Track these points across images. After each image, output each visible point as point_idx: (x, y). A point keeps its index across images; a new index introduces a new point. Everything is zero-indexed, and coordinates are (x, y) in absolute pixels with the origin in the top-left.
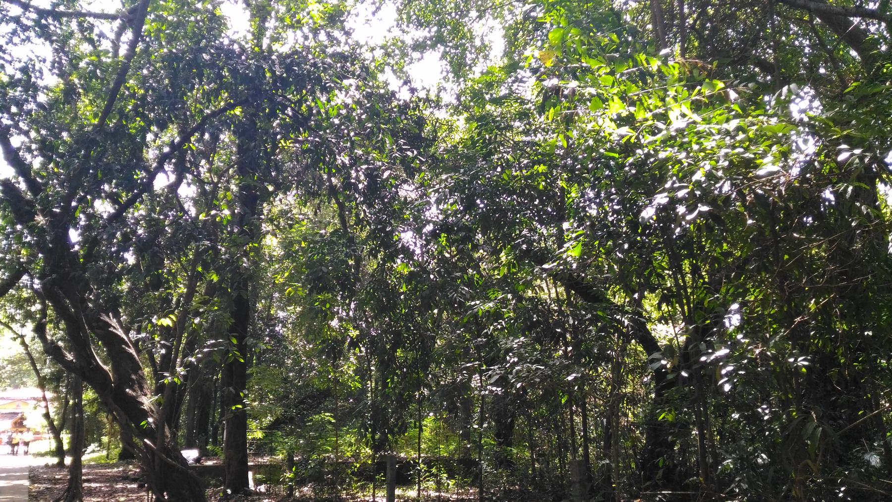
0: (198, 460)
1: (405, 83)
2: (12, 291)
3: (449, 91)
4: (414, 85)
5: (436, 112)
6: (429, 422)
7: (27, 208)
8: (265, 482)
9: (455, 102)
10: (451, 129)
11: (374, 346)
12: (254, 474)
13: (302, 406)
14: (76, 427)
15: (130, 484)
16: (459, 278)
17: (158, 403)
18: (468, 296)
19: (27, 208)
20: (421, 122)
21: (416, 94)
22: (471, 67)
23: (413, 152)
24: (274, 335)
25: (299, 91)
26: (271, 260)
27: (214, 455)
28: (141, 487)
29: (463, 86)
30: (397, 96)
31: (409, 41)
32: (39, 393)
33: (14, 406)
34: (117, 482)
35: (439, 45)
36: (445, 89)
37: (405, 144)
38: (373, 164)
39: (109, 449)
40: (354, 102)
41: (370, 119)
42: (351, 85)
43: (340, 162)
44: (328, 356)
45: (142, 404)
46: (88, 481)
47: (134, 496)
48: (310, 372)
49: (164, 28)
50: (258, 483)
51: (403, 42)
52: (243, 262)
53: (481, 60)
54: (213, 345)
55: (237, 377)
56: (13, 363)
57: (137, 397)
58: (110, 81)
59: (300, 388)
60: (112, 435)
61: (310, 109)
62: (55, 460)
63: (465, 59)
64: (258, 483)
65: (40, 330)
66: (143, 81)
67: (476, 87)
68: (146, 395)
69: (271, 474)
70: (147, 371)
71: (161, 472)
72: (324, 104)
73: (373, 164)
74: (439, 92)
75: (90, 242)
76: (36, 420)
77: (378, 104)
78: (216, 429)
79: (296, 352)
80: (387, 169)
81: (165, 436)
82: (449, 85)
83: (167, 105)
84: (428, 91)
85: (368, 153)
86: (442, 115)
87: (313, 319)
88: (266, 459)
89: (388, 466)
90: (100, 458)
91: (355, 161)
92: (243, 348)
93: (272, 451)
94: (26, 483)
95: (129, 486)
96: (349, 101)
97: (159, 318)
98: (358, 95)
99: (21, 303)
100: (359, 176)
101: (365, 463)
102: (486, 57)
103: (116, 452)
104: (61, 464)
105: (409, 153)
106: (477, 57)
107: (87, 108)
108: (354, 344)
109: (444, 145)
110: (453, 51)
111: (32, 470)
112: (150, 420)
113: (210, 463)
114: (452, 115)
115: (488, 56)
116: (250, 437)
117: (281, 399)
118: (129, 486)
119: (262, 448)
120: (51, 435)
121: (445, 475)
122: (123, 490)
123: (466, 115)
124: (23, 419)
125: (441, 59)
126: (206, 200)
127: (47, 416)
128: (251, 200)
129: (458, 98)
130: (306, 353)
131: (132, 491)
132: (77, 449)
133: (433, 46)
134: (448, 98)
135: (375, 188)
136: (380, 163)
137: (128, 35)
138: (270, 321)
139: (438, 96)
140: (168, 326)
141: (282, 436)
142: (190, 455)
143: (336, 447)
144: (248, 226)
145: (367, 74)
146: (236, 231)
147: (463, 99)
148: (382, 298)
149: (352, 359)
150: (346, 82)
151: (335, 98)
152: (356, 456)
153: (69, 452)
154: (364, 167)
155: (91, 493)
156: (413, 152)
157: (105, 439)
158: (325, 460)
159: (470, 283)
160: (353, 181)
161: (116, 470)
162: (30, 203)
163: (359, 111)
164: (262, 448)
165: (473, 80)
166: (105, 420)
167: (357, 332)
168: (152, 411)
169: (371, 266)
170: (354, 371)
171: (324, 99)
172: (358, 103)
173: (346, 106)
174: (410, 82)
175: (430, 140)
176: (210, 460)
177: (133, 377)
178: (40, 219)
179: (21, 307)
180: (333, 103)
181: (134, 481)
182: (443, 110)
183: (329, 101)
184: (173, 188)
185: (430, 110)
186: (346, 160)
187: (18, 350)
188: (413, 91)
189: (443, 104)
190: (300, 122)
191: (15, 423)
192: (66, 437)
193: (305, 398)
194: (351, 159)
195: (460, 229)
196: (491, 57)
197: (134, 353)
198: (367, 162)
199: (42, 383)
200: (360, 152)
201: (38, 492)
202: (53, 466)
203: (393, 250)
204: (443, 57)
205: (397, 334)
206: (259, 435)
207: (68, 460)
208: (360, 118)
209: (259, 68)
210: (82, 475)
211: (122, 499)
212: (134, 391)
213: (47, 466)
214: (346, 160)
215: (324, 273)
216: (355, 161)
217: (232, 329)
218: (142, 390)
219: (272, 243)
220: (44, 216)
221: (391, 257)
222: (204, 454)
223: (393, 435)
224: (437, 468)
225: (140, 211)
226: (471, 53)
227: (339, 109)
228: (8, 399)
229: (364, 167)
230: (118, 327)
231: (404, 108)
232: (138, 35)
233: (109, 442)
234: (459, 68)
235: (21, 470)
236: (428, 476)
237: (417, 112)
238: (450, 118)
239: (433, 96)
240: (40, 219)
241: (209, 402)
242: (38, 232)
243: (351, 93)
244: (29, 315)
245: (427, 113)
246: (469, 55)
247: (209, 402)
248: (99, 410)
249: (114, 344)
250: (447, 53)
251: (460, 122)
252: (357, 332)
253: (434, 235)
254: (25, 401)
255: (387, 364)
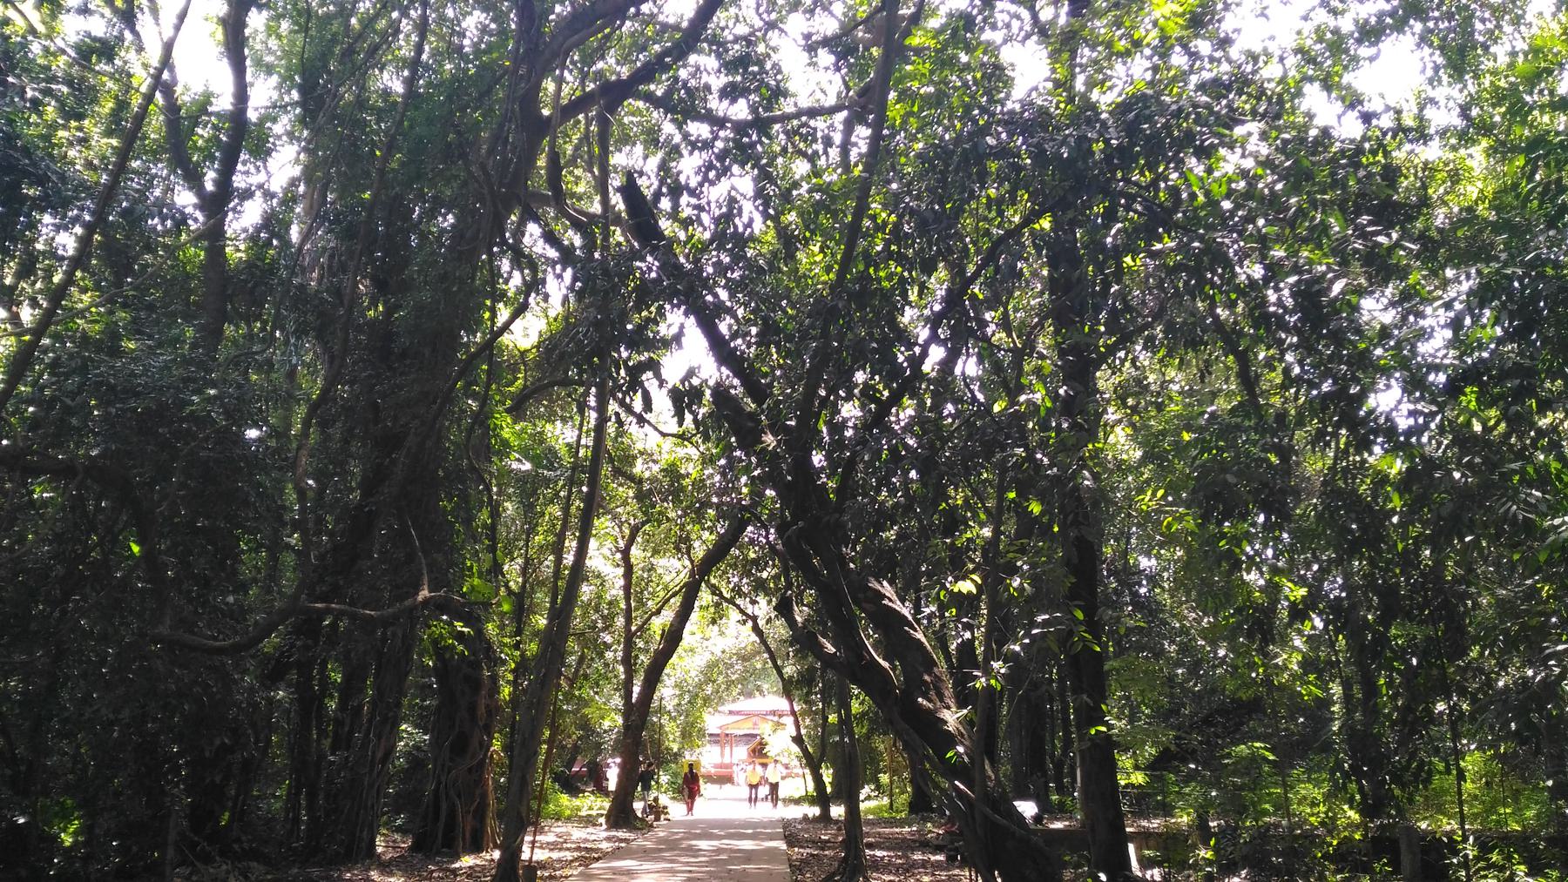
0: (1038, 819)
1: (1352, 106)
2: (734, 552)
3: (1442, 103)
4: (1368, 107)
5: (1419, 148)
6: (1472, 762)
7: (750, 424)
8: (1159, 864)
9: (1458, 122)
10: (1455, 177)
11: (1342, 616)
12: (1138, 849)
13: (1207, 727)
14: (839, 760)
15: (934, 854)
16: (1515, 472)
17: (967, 722)
18: (1543, 508)
19: (750, 424)
20: (1391, 174)
21: (1374, 122)
22: (1486, 48)
23: (1389, 236)
24: (1139, 604)
25: (1151, 167)
26: (1122, 467)
27: (1061, 811)
28: (951, 859)
29: (1472, 88)
30: (1335, 133)
31: (1346, 25)
32: (782, 704)
33: (750, 725)
34: (913, 850)
35: (1412, 22)
36: (1433, 101)
37: (1370, 223)
38: (1309, 272)
39: (891, 796)
40: (1259, 163)
41: (1294, 189)
42: (1250, 134)
43: (1243, 277)
44: (1250, 636)
45: (946, 722)
46: (871, 846)
47: (943, 875)
48: (1214, 667)
49: (916, 109)
50: (1146, 864)
51: (1336, 32)
52: (1085, 479)
53: (1508, 29)
54: (1045, 623)
55: (1089, 678)
56: (744, 658)
57: (936, 710)
58: (841, 211)
59: (1198, 697)
60: (894, 772)
61: (1174, 192)
62: (815, 811)
63: (1472, 34)
64: (1146, 864)
65: (784, 609)
66: (892, 203)
67: (1502, 83)
68: (948, 708)
69: (1171, 850)
70: (942, 666)
71: (983, 835)
72: (1201, 179)
73: (1309, 272)
74: (1421, 109)
75: (843, 466)
76: (781, 743)
77: (1305, 159)
78: (1059, 766)
79: (1184, 631)
80: (1337, 278)
81: (986, 778)
82: (1440, 93)
83: (933, 236)
84: (1398, 112)
85: (1296, 254)
86: (1432, 152)
87: (1210, 570)
88: (1155, 824)
89: (1403, 847)
90: (880, 808)
91: (1274, 272)
92: (1094, 627)
93: (1166, 810)
94: (782, 845)
95: (933, 858)
96: (1249, 163)
97: (957, 580)
98: (1264, 150)
99: (747, 567)
100: (1280, 296)
101: (1349, 839)
102: (1517, 21)
103: (903, 799)
104: (825, 817)
105: (1381, 239)
106: (1498, 27)
107: (814, 260)
108: (1299, 613)
109: (1444, 210)
110: (1443, 25)
111: (786, 824)
112: (961, 749)
113: (1058, 825)
114: (1454, 149)
115: (1522, 17)
116: (1123, 783)
117: (1165, 715)
118: (933, 858)
119: (1144, 802)
120: (807, 771)
121: (1522, 867)
122: (924, 864)
123: (1485, 143)
124: (762, 745)
125: (1418, 45)
126: (1005, 379)
127: (798, 740)
128: (1079, 367)
129: (1464, 111)
130: (1204, 633)
131: (937, 866)
132: (847, 792)
133: (1400, 26)
134: (1443, 117)
135: (1319, 316)
136: (1324, 268)
137: (862, 133)
138: (1128, 575)
139: (1420, 118)
140: (970, 593)
141: (1176, 783)
142: (1027, 809)
143: (1282, 806)
144: (1080, 411)
145: (1275, 108)
146: (1065, 425)
147: (1475, 112)
148: (1350, 520)
149: (1298, 642)
150: (1239, 131)
151: (1222, 164)
152: (1330, 825)
153: (837, 797)
154: (1292, 279)
155: (877, 865)
156: (1389, 236)
157: (884, 778)
158: (1268, 830)
159: (1542, 479)
160: (1272, 309)
161: (907, 829)
162: (753, 416)
163: (1269, 179)
164: (1144, 802)
165: (1494, 73)
166: (882, 747)
167: (1303, 591)
168: (962, 735)
169: (1315, 465)
170: (1301, 664)
171: (1200, 170)
172: (1267, 163)
173: (1244, 174)
174: (1361, 103)
175: (1412, 207)
176: (1058, 820)
177: (927, 678)
178: (769, 439)
179: (748, 574)
180: (1217, 174)
181: (938, 849)
182: (1435, 143)
183: (1209, 171)
184: (947, 365)
185: (1407, 147)
186: (1258, 272)
187: (747, 637)
188: (1367, 118)
189: (1432, 131)
190: (1158, 218)
191: (754, 751)
192: (827, 775)
193: (1211, 715)
194: (1266, 268)
195: (1504, 375)
196: (1529, 17)
197: (924, 640)
198: (1296, 269)
199: (787, 693)
200: (1281, 253)
201: (801, 861)
202: (816, 820)
203: (1364, 430)
204: (1424, 40)
205: (1389, 594)
206: (1139, 778)
207: (838, 811)
208: (1271, 190)
209: (1083, 140)
210: (862, 835)
211: (926, 879)
212: (930, 701)
213: (805, 818)
214: (1258, 272)
215: (1230, 481)
216: (1274, 272)
217: (1073, 595)
218: (942, 701)
219: (1120, 442)
220: (775, 434)
221: (1365, 445)
222: (1046, 809)
223: (1403, 786)
224: (1501, 852)
225: (907, 411)
226: (1483, 21)
227: (1230, 181)
228: (738, 713)
229: (1292, 279)
230: (895, 598)
231: (1355, 153)
232: (877, 126)
233: (892, 782)
234: (1459, 57)
235: (772, 824)
236: (1484, 869)
237: (1380, 157)
238: (1451, 156)
239: (1409, 121)
240: (769, 439)
241: (1045, 720)
242: (765, 457)
243: (1250, 148)
244: (760, 586)
245: (1399, 155)
246: (1479, 26)
247: (1045, 720)
248: (871, 732)
249: (890, 623)
250: (1431, 31)
251: (1477, 157)
252: (1303, 591)
253: (1453, 389)
254: (763, 715)
255: (1370, 652)
